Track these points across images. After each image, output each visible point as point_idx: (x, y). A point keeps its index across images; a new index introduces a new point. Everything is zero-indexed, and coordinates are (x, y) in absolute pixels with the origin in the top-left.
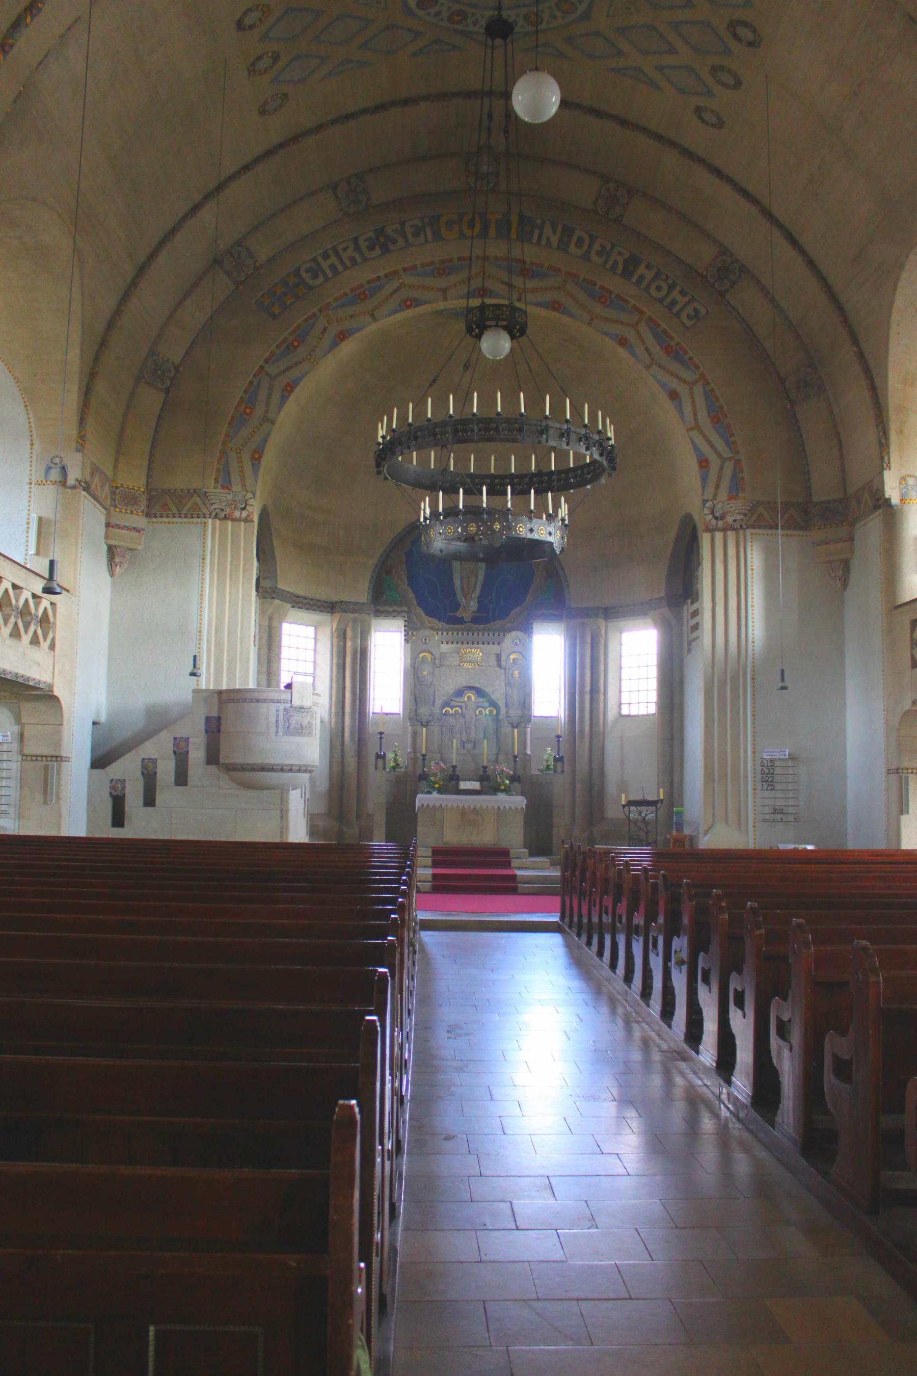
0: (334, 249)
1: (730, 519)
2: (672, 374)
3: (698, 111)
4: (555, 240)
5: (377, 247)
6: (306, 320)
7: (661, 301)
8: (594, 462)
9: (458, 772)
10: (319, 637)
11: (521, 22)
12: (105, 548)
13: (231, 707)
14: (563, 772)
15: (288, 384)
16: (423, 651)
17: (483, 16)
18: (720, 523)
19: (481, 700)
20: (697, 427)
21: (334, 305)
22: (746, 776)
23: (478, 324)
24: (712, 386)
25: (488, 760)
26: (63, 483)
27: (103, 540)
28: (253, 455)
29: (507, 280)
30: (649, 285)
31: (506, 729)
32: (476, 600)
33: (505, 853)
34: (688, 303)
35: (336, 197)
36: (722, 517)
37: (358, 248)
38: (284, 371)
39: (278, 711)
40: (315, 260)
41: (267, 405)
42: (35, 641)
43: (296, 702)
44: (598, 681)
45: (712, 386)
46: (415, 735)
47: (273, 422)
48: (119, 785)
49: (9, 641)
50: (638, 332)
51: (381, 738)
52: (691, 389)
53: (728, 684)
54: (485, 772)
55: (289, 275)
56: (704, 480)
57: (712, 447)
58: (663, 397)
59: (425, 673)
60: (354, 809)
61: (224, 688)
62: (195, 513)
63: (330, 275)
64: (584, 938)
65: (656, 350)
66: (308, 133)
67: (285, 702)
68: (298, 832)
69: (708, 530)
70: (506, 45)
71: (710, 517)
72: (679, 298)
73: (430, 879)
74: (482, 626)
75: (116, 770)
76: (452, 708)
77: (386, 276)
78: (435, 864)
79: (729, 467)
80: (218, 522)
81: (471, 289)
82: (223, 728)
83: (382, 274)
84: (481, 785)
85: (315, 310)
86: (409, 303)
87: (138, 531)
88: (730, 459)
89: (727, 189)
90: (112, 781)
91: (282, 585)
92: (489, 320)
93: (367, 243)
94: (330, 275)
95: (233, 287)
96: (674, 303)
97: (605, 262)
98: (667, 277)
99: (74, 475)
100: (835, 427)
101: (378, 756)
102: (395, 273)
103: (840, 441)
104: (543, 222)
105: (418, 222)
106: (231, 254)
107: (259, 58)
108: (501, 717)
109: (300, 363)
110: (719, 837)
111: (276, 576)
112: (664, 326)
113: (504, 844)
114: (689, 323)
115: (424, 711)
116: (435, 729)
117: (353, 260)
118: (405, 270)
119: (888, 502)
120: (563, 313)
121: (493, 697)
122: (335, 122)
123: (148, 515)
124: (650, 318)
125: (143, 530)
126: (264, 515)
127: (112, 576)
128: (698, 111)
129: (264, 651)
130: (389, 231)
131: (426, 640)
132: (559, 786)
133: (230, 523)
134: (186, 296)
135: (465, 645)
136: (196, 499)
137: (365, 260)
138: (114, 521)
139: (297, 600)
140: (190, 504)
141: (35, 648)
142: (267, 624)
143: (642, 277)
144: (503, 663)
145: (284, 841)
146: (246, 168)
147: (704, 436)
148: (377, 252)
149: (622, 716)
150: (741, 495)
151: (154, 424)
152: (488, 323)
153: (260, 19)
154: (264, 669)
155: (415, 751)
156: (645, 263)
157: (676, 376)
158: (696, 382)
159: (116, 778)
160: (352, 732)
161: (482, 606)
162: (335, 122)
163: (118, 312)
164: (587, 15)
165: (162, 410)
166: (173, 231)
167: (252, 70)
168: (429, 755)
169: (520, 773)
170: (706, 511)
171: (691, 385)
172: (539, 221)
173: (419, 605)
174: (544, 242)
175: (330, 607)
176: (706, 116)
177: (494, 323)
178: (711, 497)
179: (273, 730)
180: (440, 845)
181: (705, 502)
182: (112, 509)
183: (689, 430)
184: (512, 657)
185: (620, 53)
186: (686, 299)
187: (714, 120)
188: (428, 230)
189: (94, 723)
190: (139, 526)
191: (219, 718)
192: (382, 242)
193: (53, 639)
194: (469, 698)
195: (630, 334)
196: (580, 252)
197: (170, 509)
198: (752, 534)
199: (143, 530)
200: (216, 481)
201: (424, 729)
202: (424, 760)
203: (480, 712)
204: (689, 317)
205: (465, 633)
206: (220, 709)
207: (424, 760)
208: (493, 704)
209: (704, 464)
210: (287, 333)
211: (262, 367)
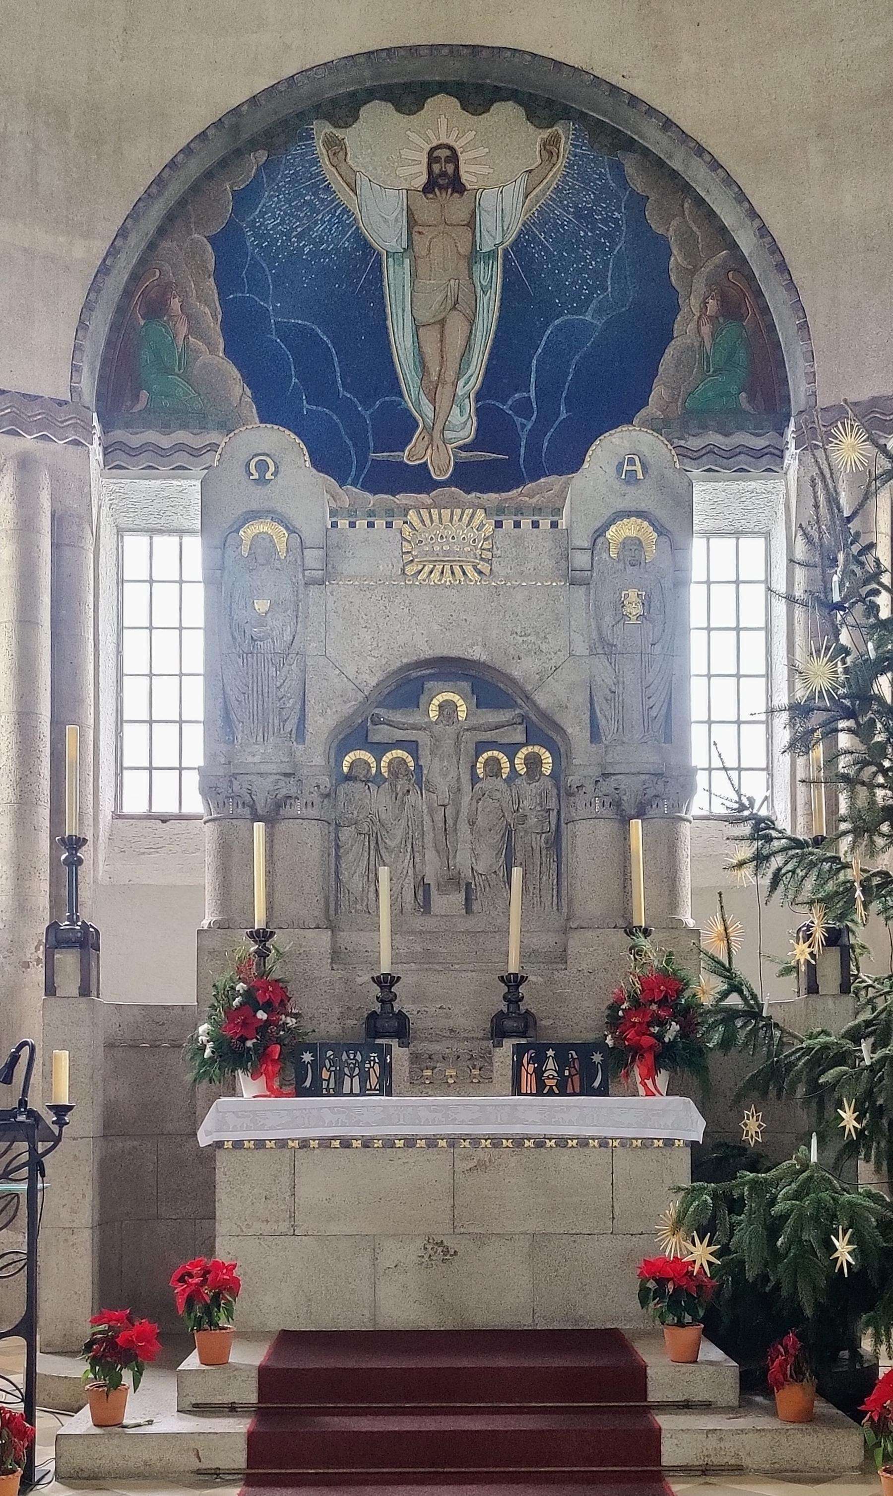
16: (253, 516)
25: (526, 955)
32: (470, 406)
33: (611, 1340)
76: (379, 749)
131: (262, 467)
161: (492, 426)
194: (447, 708)
203: (493, 767)
208: (542, 730)
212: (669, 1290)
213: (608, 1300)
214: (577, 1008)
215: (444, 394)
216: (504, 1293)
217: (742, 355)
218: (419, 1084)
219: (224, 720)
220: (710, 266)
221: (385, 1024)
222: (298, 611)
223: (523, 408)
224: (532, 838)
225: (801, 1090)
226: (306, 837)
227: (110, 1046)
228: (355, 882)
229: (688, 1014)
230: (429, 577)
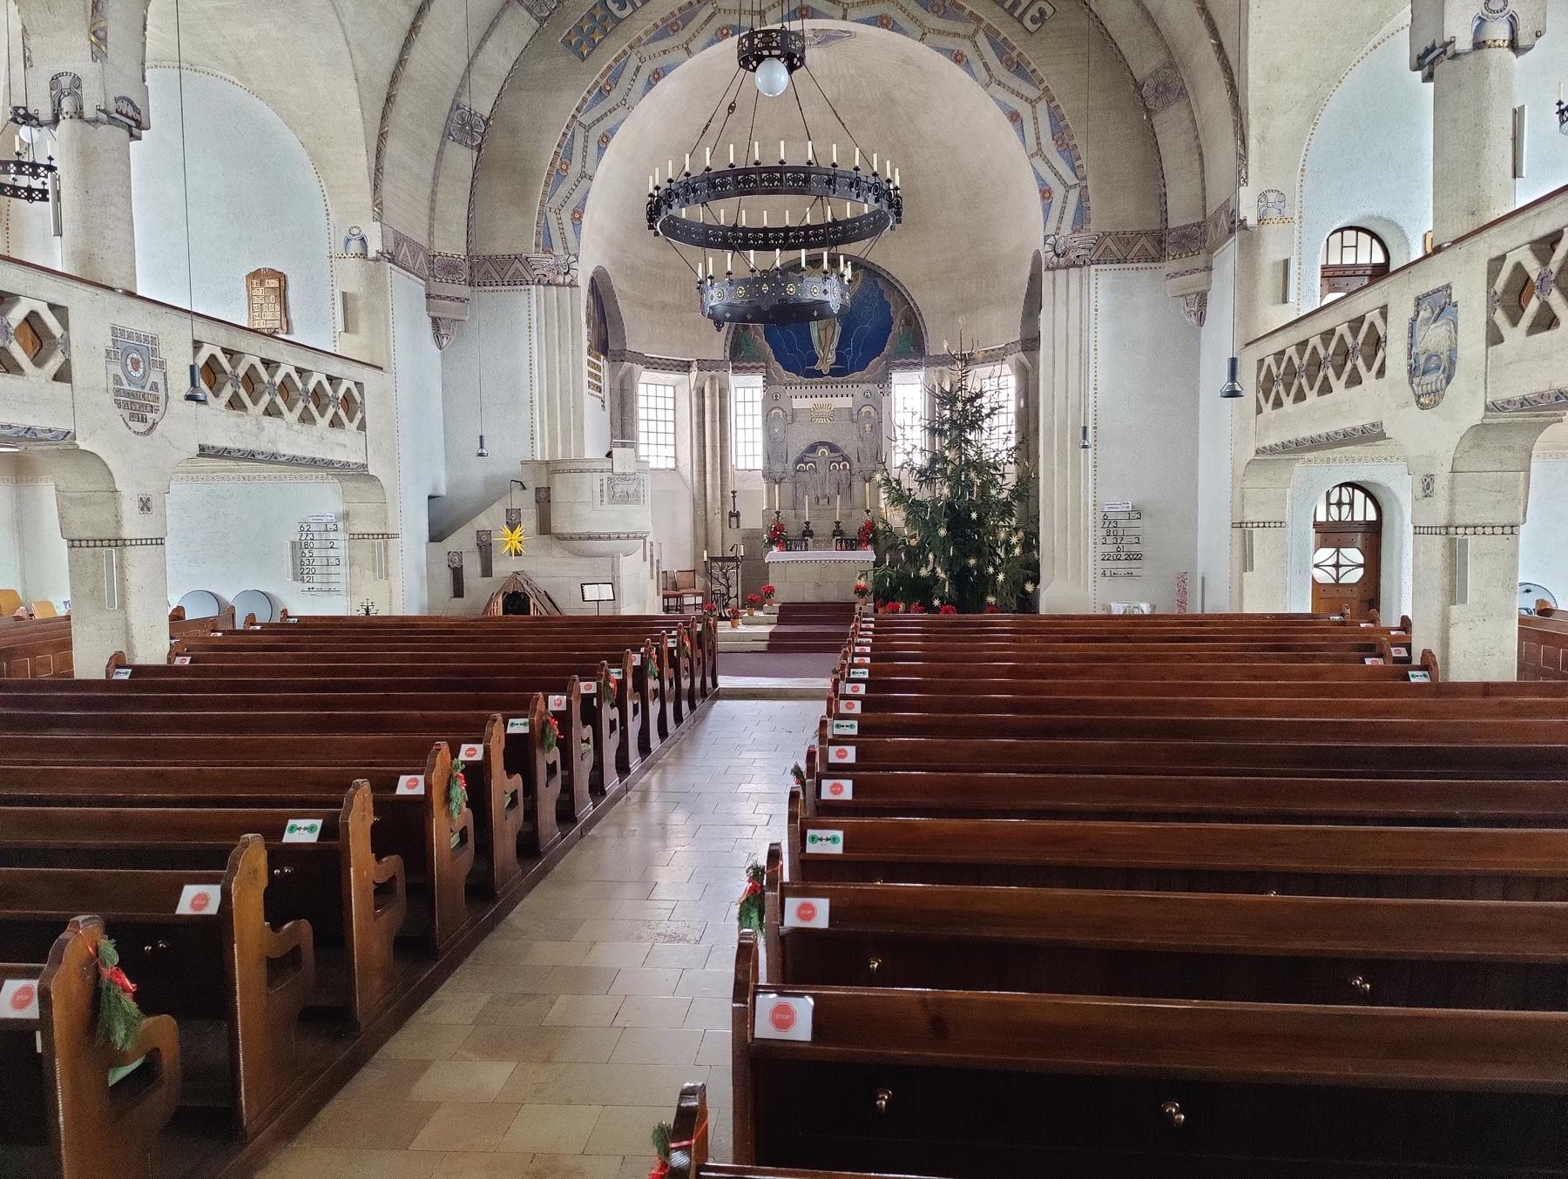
1: (1072, 256)
6: (616, 60)
18: (1062, 260)
26: (364, 255)
42: (335, 423)
49: (298, 427)
50: (975, 45)
62: (518, 281)
65: (994, 63)
69: (1048, 268)
75: (451, 543)
78: (780, 621)
79: (1074, 196)
99: (374, 246)
100: (1197, 137)
101: (731, 515)
103: (1201, 155)
112: (1004, 34)
114: (1032, 27)
115: (778, 468)
129: (617, 414)
134: (484, 40)
136: (517, 264)
138: (434, 292)
140: (512, 270)
141: (337, 430)
147: (1048, 162)
161: (840, 358)
163: (401, 62)
170: (1048, 248)
181: (1046, 238)
189: (430, 497)
193: (363, 418)
195: (966, 48)
200: (537, 245)
204: (1033, 20)
208: (845, 458)
212: (861, 592)
213: (853, 597)
214: (852, 530)
216: (832, 594)
218: (815, 548)
219: (769, 457)
221: (807, 533)
225: (341, 549)
226: (788, 486)
229: (875, 532)
230: (822, 405)
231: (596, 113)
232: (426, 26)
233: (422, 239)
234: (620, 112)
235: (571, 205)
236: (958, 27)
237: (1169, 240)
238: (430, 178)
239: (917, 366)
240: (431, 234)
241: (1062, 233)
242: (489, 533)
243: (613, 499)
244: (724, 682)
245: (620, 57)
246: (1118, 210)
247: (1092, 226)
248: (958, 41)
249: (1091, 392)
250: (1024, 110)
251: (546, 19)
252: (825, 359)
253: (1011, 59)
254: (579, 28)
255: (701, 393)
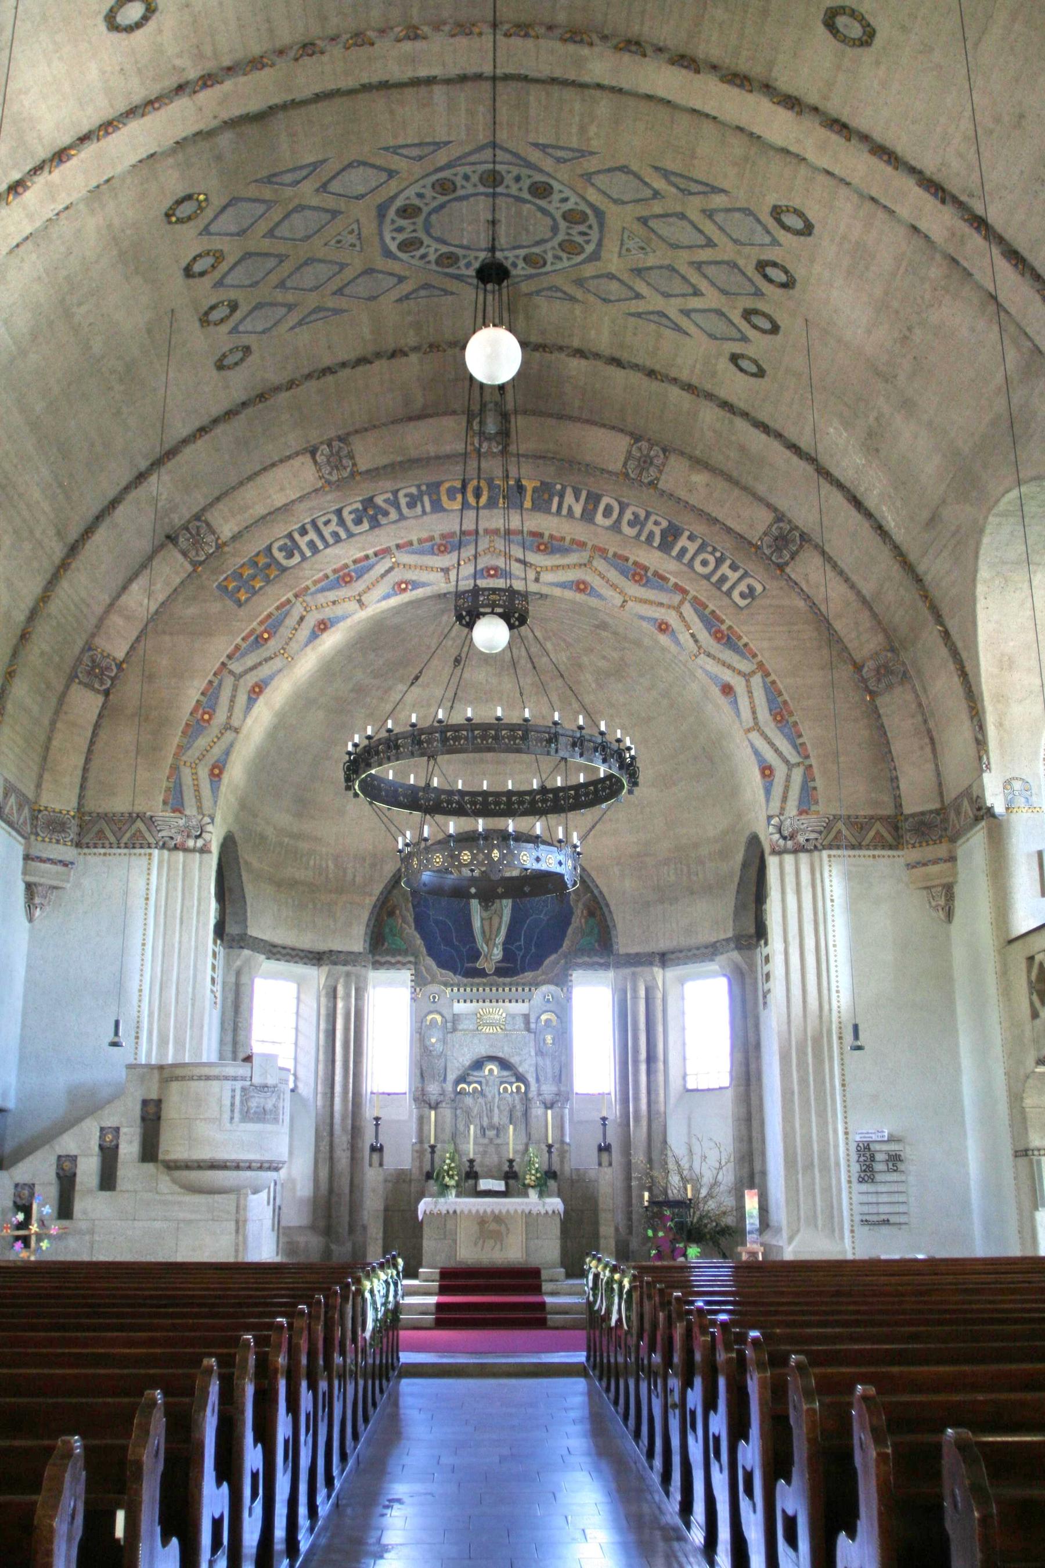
0: (314, 523)
1: (801, 839)
2: (724, 664)
3: (734, 358)
4: (578, 510)
5: (365, 520)
6: (278, 608)
7: (707, 577)
8: (609, 777)
9: (477, 1168)
10: (302, 996)
11: (521, 264)
12: (21, 887)
13: (175, 1086)
14: (610, 1164)
15: (257, 685)
17: (476, 258)
18: (790, 843)
19: (505, 1073)
20: (756, 727)
21: (313, 589)
22: (838, 1164)
23: (468, 610)
24: (773, 677)
25: (515, 1152)
27: (20, 876)
28: (212, 770)
29: (521, 557)
30: (693, 559)
31: (537, 1110)
32: (500, 947)
33: (534, 1274)
34: (740, 579)
35: (315, 462)
36: (792, 837)
37: (342, 522)
38: (252, 669)
39: (233, 1091)
40: (290, 536)
41: (231, 709)
43: (256, 1080)
44: (655, 1046)
45: (773, 677)
46: (422, 1120)
47: (237, 731)
48: (26, 1192)
50: (681, 615)
51: (377, 1125)
52: (748, 681)
53: (812, 1047)
54: (511, 1166)
55: (258, 554)
56: (768, 791)
57: (776, 750)
58: (716, 691)
59: (433, 1040)
60: (346, 1219)
61: (170, 1060)
63: (308, 554)
64: (604, 1383)
65: (704, 636)
66: (277, 389)
67: (243, 1079)
68: (264, 1249)
69: (774, 852)
70: (500, 290)
71: (777, 836)
72: (729, 573)
73: (433, 1309)
74: (508, 980)
75: (21, 1172)
77: (376, 554)
78: (443, 1290)
79: (797, 775)
80: (166, 852)
81: (479, 568)
82: (164, 1114)
83: (370, 552)
84: (507, 1184)
85: (290, 595)
86: (403, 586)
87: (66, 865)
88: (798, 764)
89: (776, 445)
90: (17, 1185)
91: (253, 931)
92: (483, 606)
93: (353, 516)
94: (308, 554)
95: (190, 568)
96: (723, 579)
97: (639, 535)
98: (715, 549)
100: (925, 721)
101: (373, 1149)
102: (386, 552)
103: (932, 739)
104: (564, 488)
105: (414, 490)
106: (187, 529)
107: (213, 308)
108: (530, 1095)
109: (271, 658)
110: (797, 1245)
111: (245, 920)
112: (711, 607)
113: (534, 1262)
114: (742, 603)
115: (433, 1089)
116: (447, 1112)
117: (335, 534)
118: (398, 546)
119: (990, 812)
120: (589, 595)
121: (521, 1070)
122: (309, 376)
123: (78, 845)
124: (695, 598)
125: (72, 863)
126: (228, 845)
127: (31, 920)
128: (734, 358)
129: (230, 1014)
130: (379, 500)
132: (607, 1181)
133: (181, 854)
135: (487, 1004)
136: (139, 824)
137: (351, 535)
138: (34, 852)
139: (275, 950)
142: (233, 980)
143: (683, 551)
144: (533, 1026)
145: (240, 1260)
146: (203, 430)
147: (766, 738)
148: (366, 526)
149: (688, 1091)
150: (813, 808)
151: (89, 734)
152: (482, 610)
153: (213, 266)
154: (229, 1038)
155: (421, 1141)
156: (687, 534)
157: (729, 667)
158: (754, 672)
159: (21, 1182)
160: (344, 1118)
161: (508, 954)
162: (309, 376)
163: (45, 598)
164: (595, 256)
165: (100, 716)
166: (113, 504)
167: (205, 320)
168: (439, 1146)
169: (556, 1167)
170: (771, 829)
171: (747, 676)
172: (558, 487)
173: (430, 955)
174: (564, 512)
175: (316, 958)
176: (744, 364)
177: (489, 610)
178: (777, 811)
179: (227, 1116)
180: (451, 1264)
181: (770, 818)
182: (33, 837)
183: (749, 730)
184: (544, 1017)
185: (638, 296)
186: (737, 575)
187: (754, 369)
188: (426, 499)
190: (67, 858)
191: (159, 1102)
192: (371, 514)
194: (491, 1071)
196: (608, 522)
197: (144, 838)
198: (829, 856)
199: (72, 863)
200: (165, 803)
201: (433, 1113)
202: (433, 1152)
203: (505, 1089)
204: (742, 595)
205: (487, 989)
206: (160, 1088)
207: (433, 1152)
208: (520, 1078)
209: (767, 772)
210: (255, 624)
211: (223, 664)
215: (491, 943)
217: (596, 931)
220: (584, 899)
222: (444, 1041)
223: (519, 948)
224: (518, 1114)
227: (386, 1181)
228: (461, 1127)
230: (487, 1017)
231: (250, 661)
232: (79, 563)
233: (31, 795)
234: (277, 663)
235: (210, 759)
236: (663, 597)
237: (906, 826)
238: (46, 722)
239: (606, 966)
240: (39, 786)
241: (787, 814)
242: (73, 1159)
243: (247, 1116)
244: (406, 1357)
245: (283, 605)
246: (852, 794)
247: (821, 808)
248: (663, 610)
249: (834, 995)
250: (738, 684)
251: (201, 563)
252: (490, 953)
253: (719, 631)
254: (238, 575)
255: (333, 994)
